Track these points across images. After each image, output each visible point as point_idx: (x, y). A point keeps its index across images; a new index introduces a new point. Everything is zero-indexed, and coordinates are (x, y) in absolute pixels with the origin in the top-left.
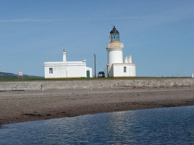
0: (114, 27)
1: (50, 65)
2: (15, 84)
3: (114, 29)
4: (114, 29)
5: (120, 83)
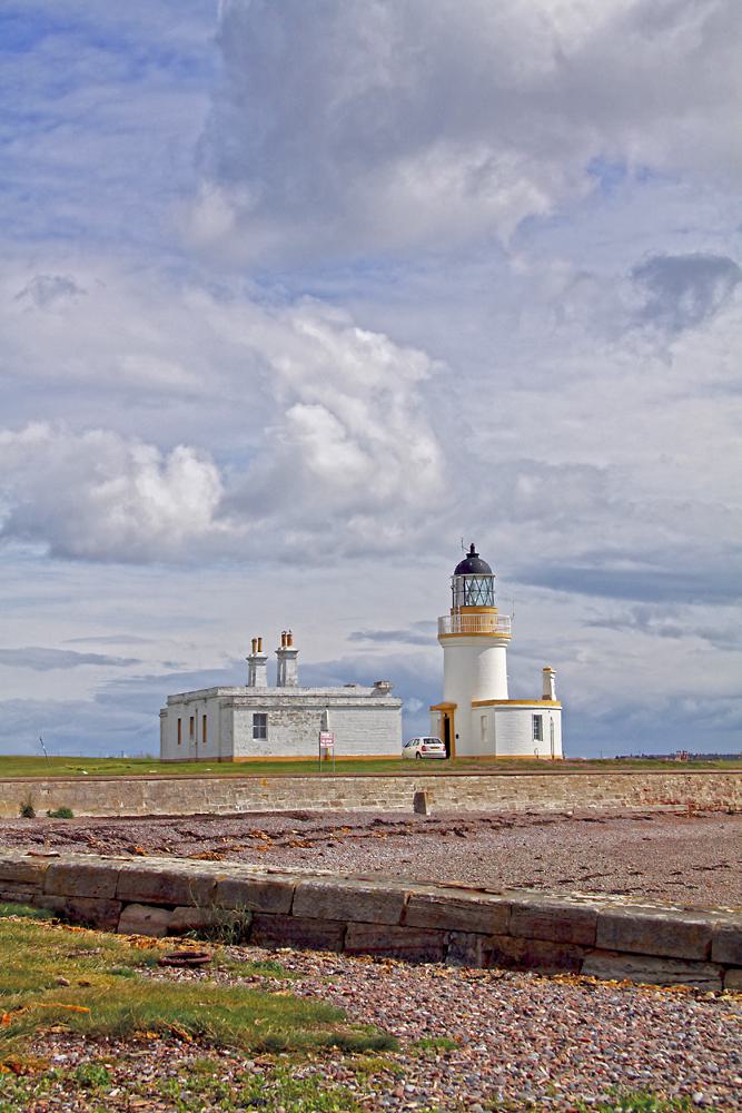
0: (472, 548)
1: (259, 702)
2: (331, 786)
3: (472, 555)
4: (472, 555)
5: (650, 787)
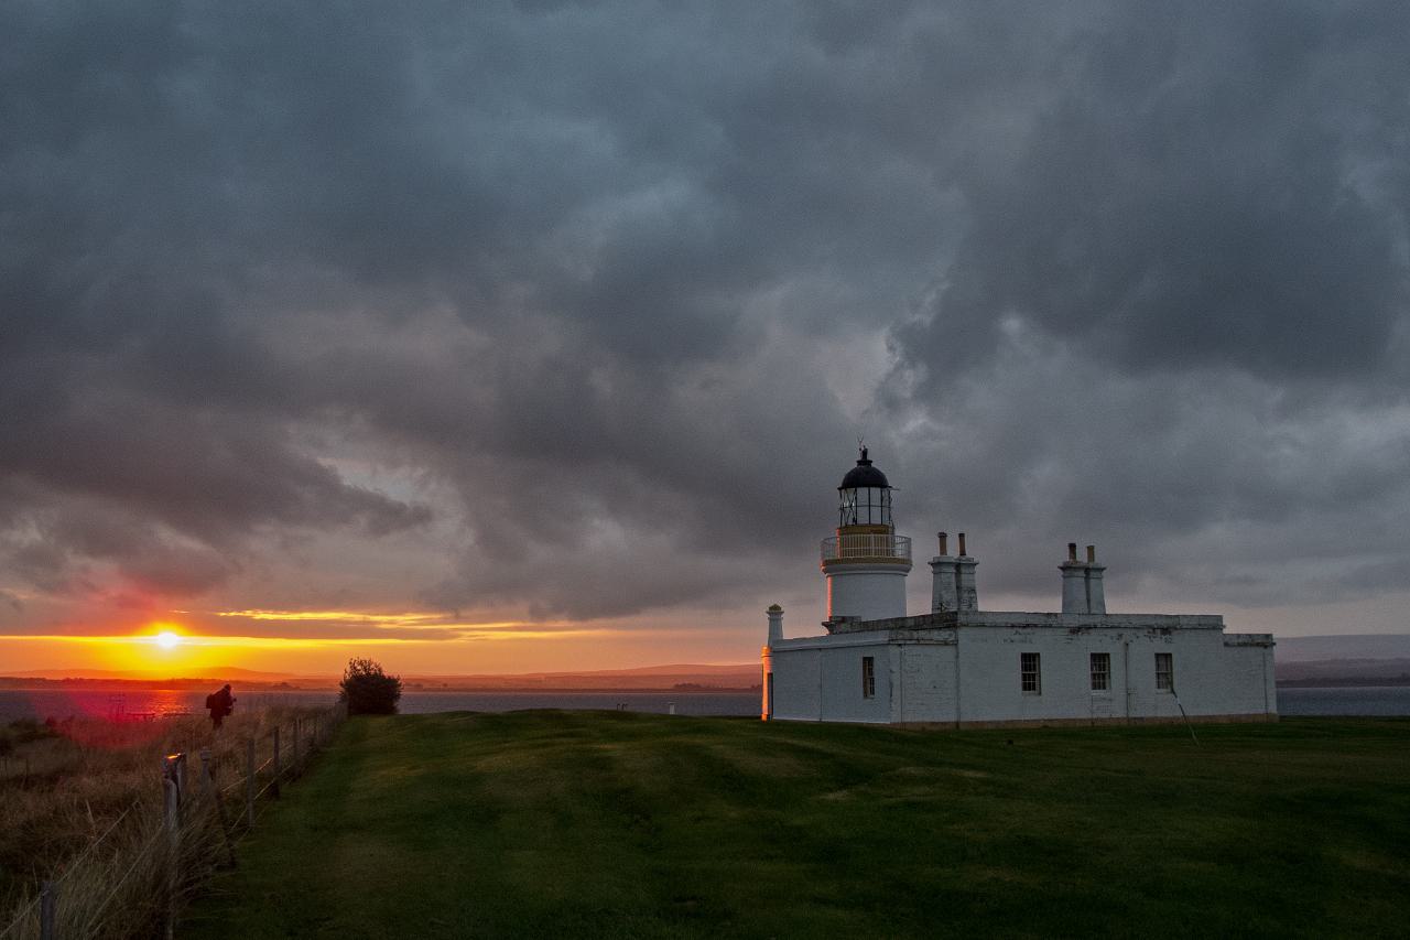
3: (865, 461)
